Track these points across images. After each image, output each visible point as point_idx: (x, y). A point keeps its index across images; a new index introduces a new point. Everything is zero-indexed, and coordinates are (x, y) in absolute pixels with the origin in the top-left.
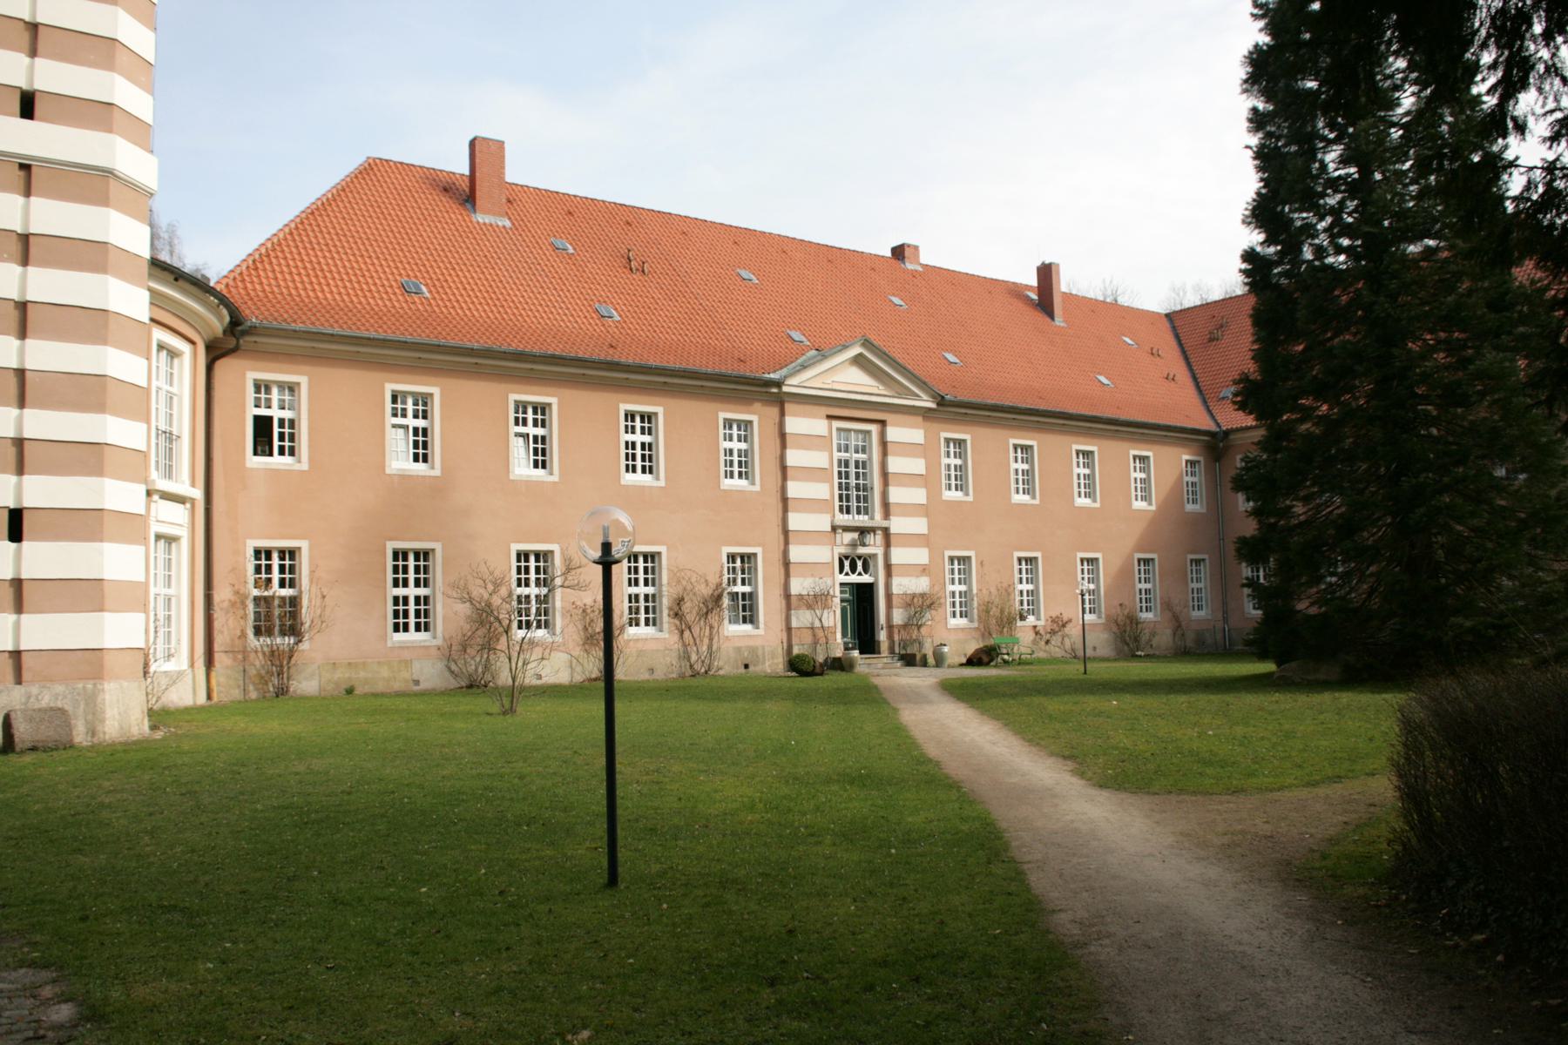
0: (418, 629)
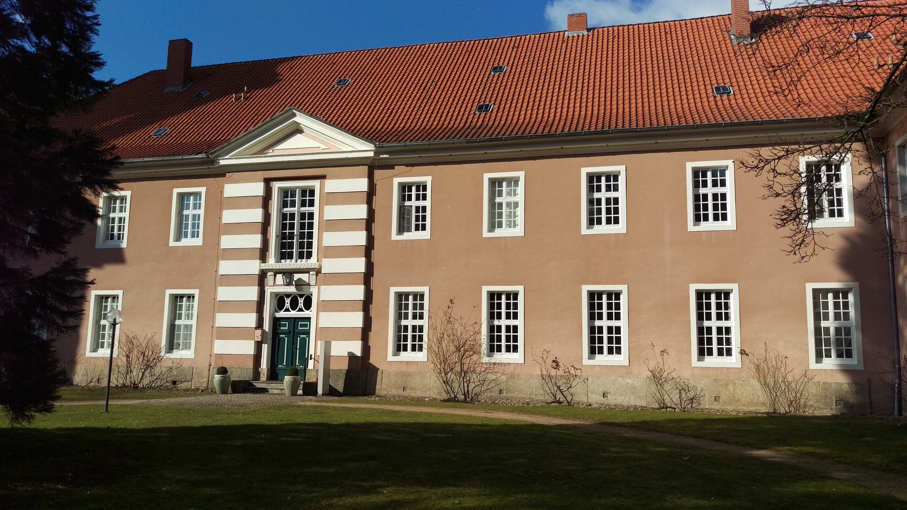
0: (716, 218)
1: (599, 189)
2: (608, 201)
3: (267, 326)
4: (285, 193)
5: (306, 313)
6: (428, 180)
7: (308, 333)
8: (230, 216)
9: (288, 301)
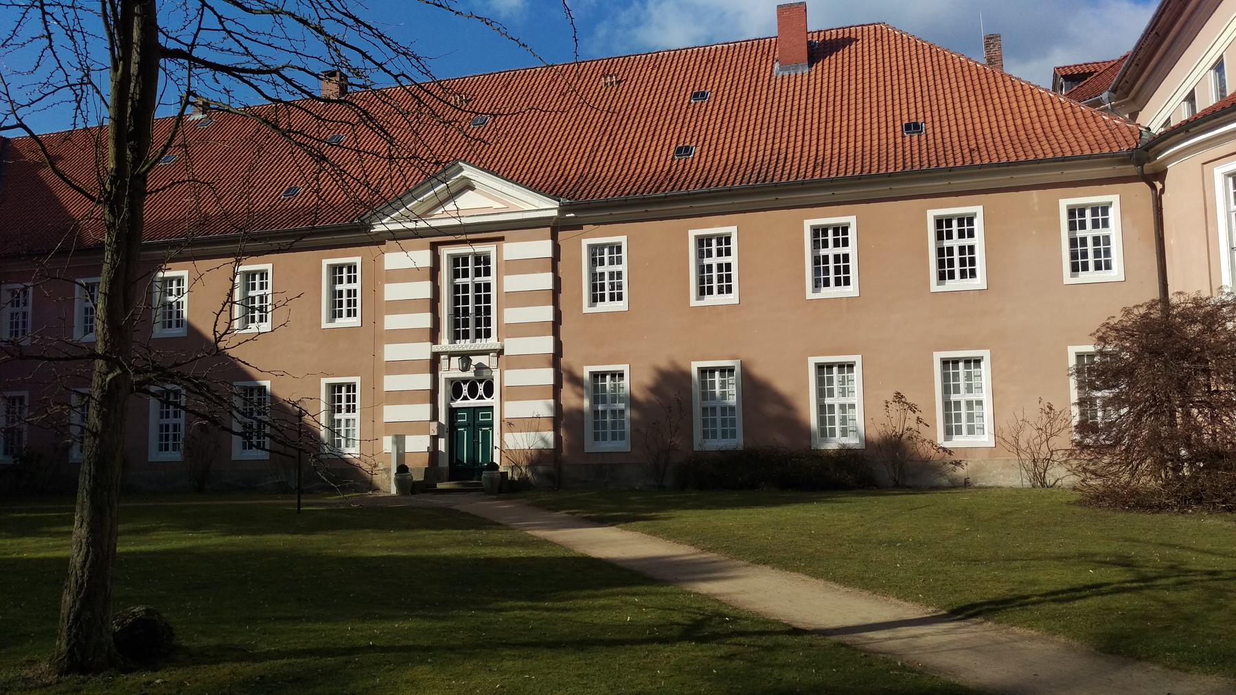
0: (838, 283)
2: (720, 267)
3: (442, 418)
4: (455, 260)
5: (487, 402)
6: (732, 230)
7: (491, 425)
8: (393, 292)
9: (465, 388)
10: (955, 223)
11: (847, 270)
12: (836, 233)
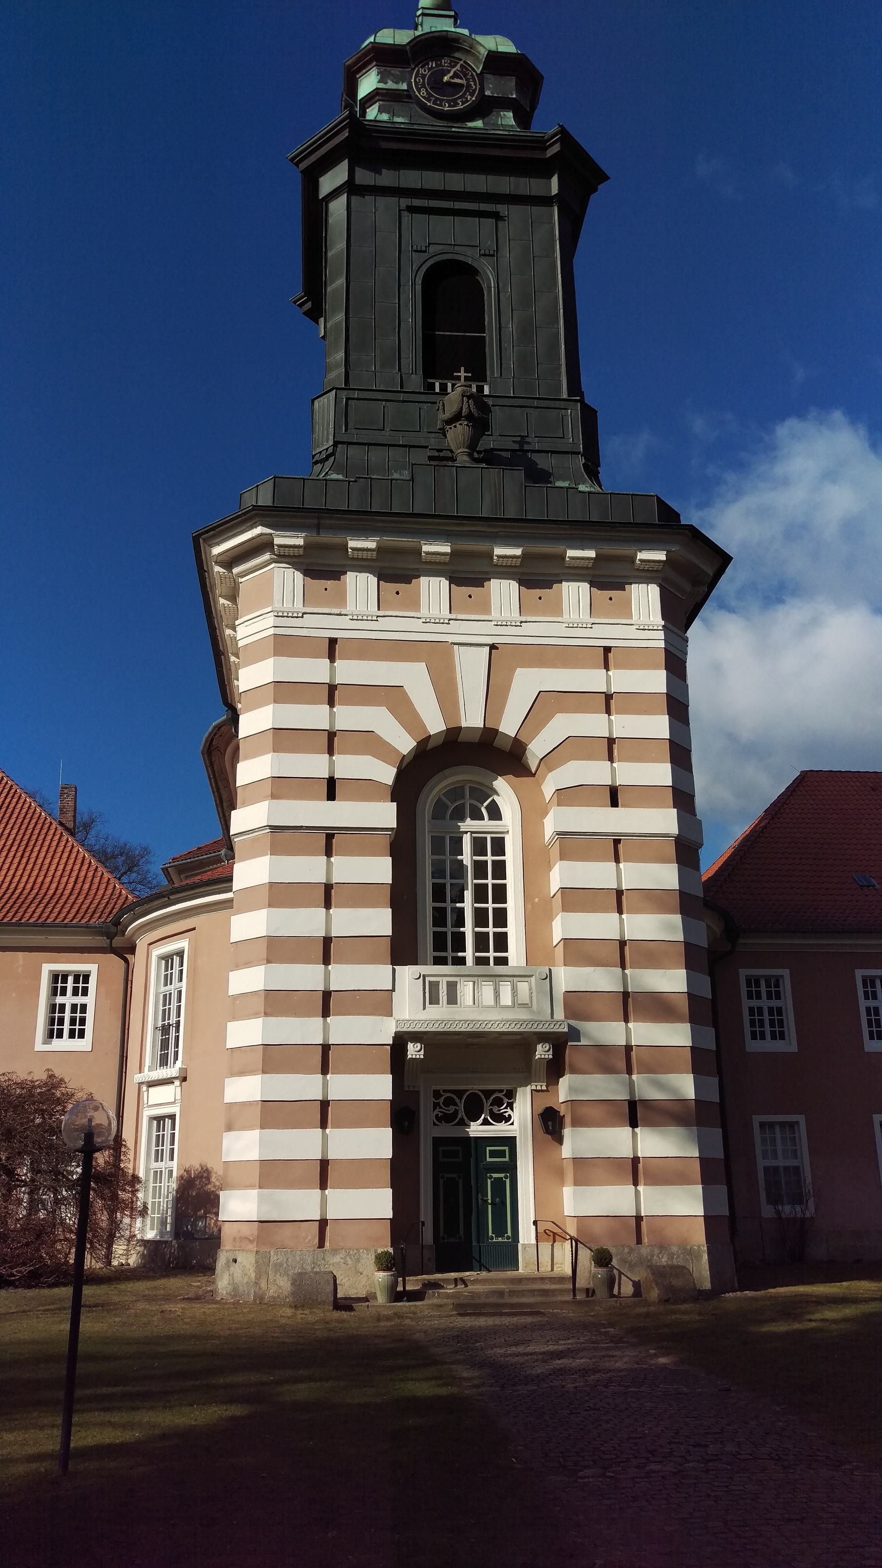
0: (72, 1035)
1: (64, 992)
6: (92, 968)
10: (70, 979)
11: (83, 1021)
12: (76, 980)
